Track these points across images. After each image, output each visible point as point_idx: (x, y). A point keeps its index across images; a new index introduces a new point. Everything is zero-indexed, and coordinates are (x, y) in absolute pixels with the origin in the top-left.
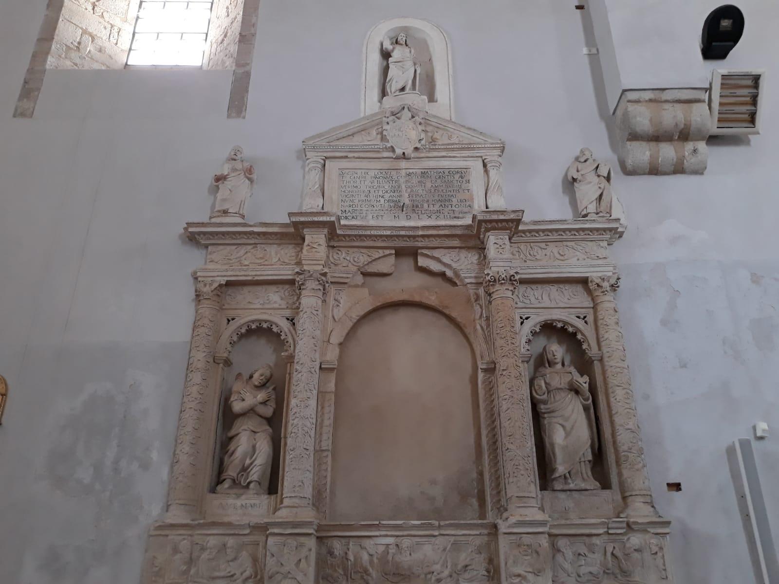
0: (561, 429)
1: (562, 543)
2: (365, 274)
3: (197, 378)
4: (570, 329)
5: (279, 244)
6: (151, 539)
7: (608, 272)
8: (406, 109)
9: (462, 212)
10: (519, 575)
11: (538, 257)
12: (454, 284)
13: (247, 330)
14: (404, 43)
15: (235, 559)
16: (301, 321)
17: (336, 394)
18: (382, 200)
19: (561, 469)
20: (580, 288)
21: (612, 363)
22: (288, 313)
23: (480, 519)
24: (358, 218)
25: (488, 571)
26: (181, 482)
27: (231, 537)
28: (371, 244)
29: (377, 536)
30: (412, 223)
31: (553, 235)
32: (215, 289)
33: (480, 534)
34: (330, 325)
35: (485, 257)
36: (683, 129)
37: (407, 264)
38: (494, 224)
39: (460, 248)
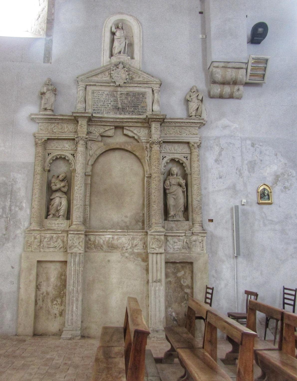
0: (173, 199)
1: (169, 238)
2: (102, 136)
3: (38, 177)
4: (181, 162)
5: (68, 123)
6: (26, 234)
7: (197, 140)
8: (121, 64)
9: (142, 112)
10: (153, 248)
11: (171, 133)
12: (138, 142)
13: (56, 158)
14: (121, 28)
15: (56, 241)
16: (78, 157)
17: (91, 184)
18: (110, 105)
19: (172, 213)
20: (186, 146)
21: (194, 176)
22: (72, 152)
23: (142, 230)
24: (100, 113)
25: (143, 247)
26: (35, 215)
27: (54, 234)
28: (105, 124)
29: (90, 235)
30: (122, 116)
31: (178, 124)
32: (43, 142)
33: (142, 235)
34: (88, 157)
35: (151, 131)
36: (234, 81)
37: (119, 132)
38: (154, 120)
39: (141, 127)
